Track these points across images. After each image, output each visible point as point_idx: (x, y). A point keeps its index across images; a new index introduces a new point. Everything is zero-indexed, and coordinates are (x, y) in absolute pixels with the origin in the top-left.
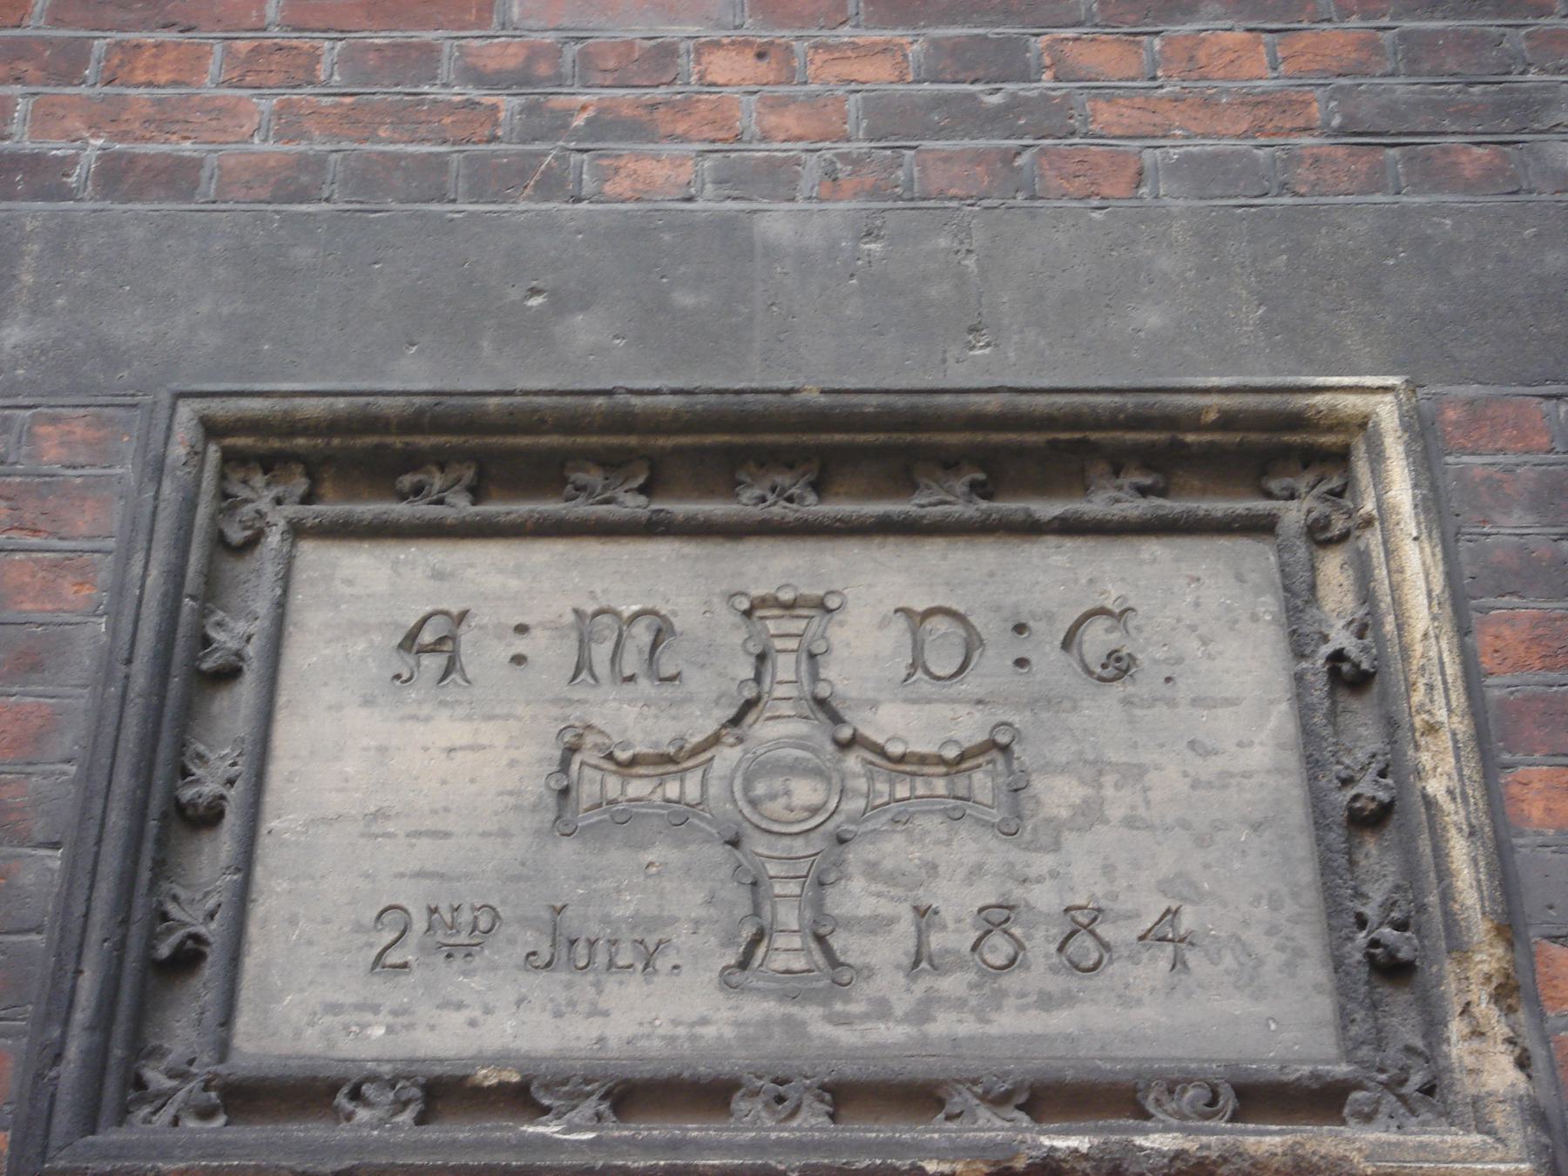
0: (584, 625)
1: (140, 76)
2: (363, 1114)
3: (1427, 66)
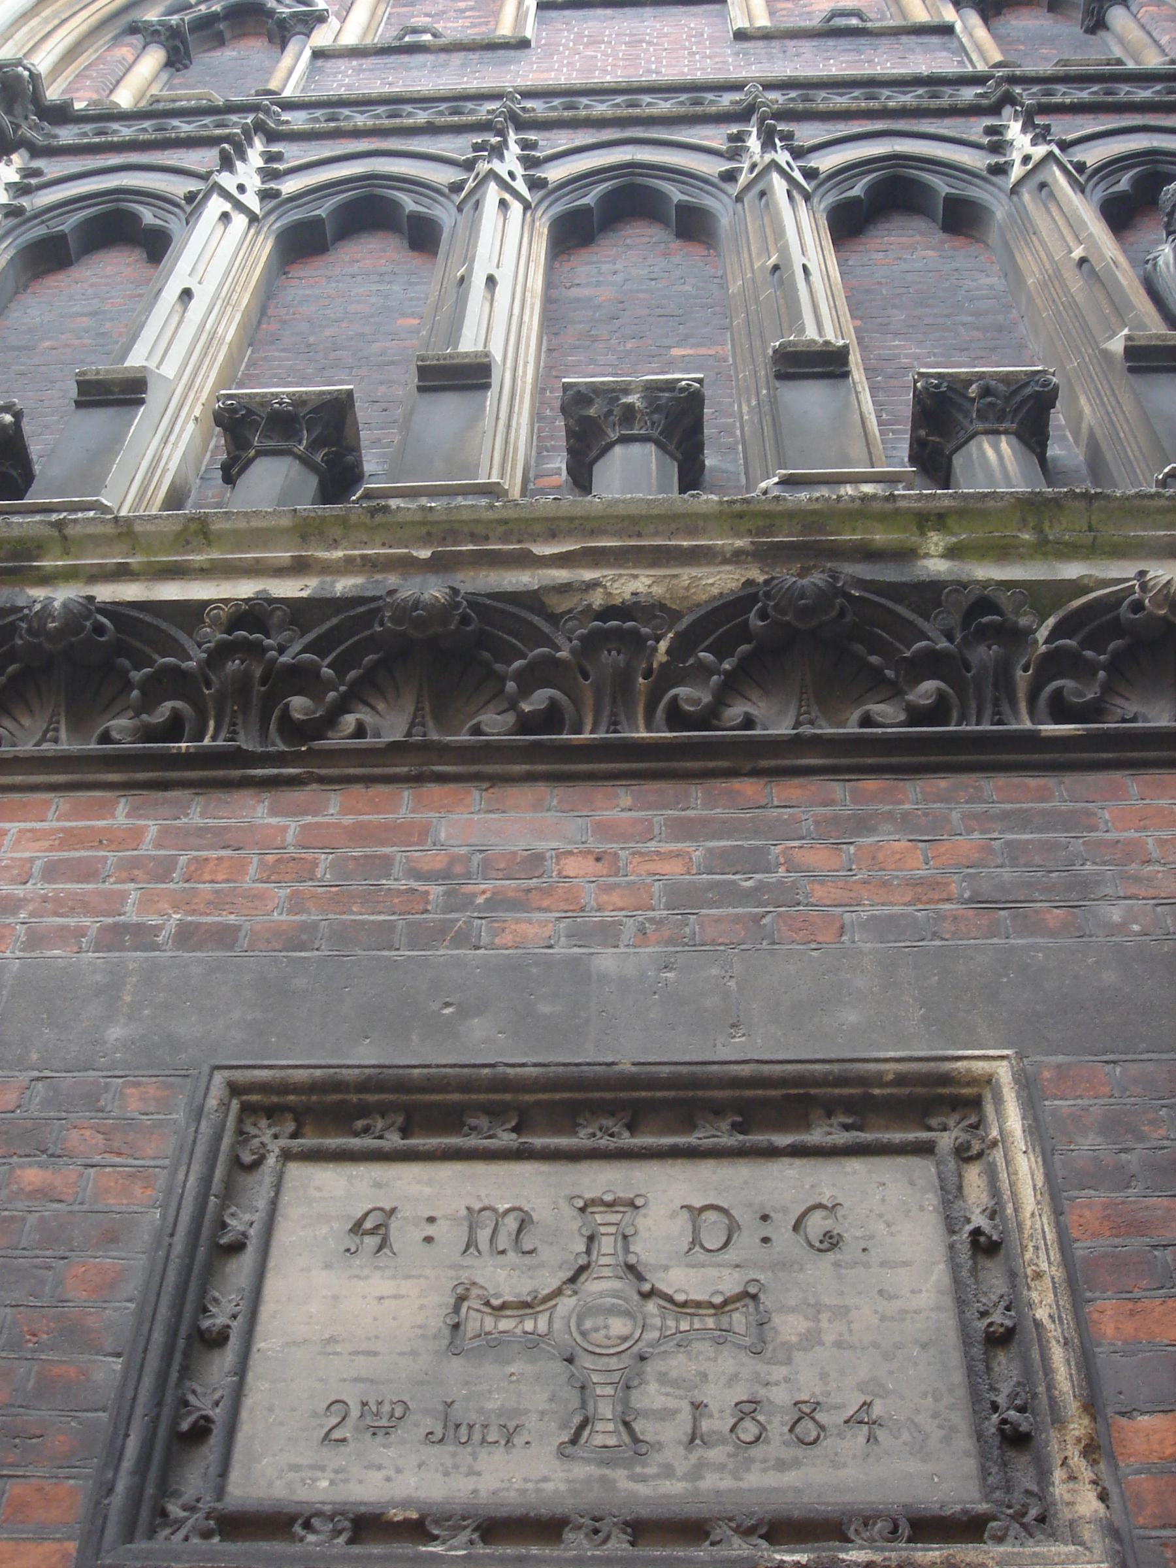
0: (473, 1217)
1: (207, 877)
2: (311, 1538)
3: (1022, 861)
